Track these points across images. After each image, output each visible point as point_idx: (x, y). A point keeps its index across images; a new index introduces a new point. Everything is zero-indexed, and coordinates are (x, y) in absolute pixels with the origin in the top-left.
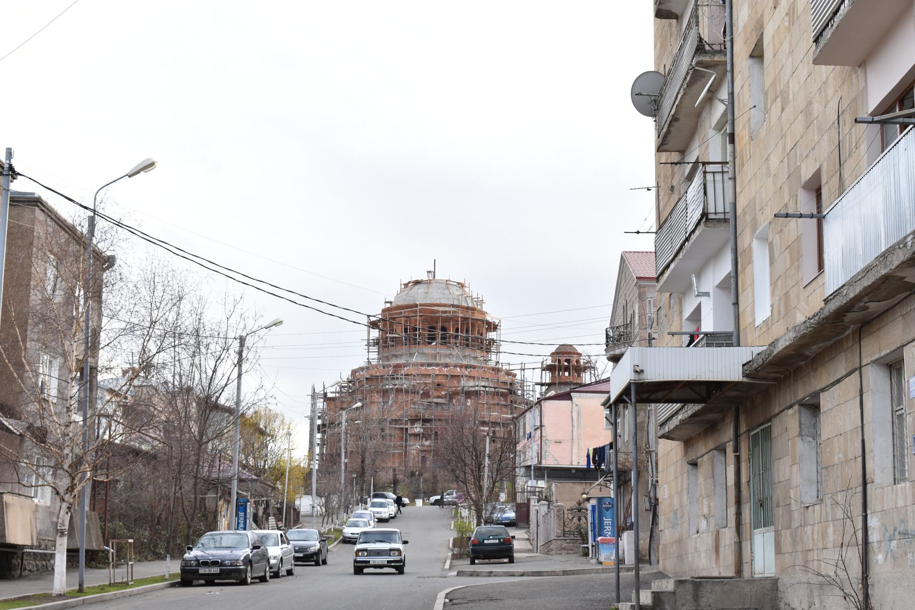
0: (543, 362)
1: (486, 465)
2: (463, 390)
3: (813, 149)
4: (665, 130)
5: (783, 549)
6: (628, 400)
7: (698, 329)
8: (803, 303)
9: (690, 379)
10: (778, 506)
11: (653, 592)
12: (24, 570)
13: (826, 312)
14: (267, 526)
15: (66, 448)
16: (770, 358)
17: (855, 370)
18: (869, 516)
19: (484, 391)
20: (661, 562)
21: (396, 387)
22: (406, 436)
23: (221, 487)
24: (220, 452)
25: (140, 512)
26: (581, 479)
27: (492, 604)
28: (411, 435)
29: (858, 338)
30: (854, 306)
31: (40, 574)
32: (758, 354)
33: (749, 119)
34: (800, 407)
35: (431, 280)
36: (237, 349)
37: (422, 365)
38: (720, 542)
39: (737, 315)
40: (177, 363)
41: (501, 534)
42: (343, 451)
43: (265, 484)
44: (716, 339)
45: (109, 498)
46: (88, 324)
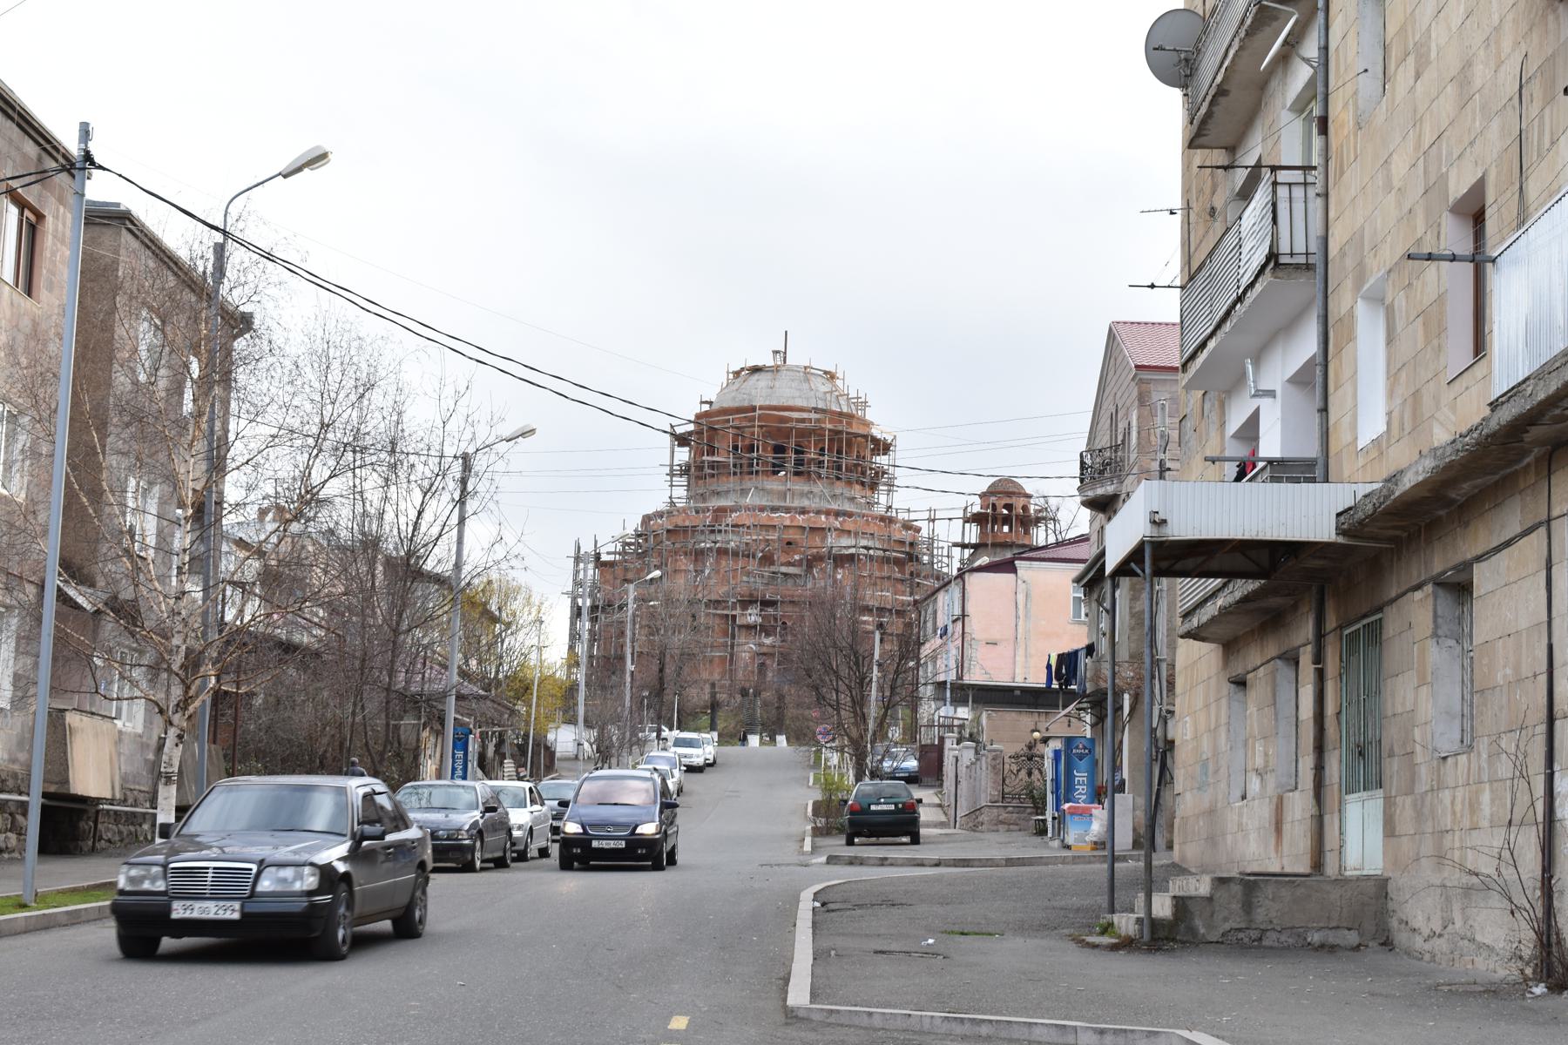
0: (966, 508)
1: (874, 679)
2: (830, 552)
3: (1471, 144)
4: (1203, 110)
5: (1398, 829)
6: (1139, 571)
7: (1254, 452)
8: (1445, 410)
9: (1246, 537)
10: (1391, 755)
11: (1174, 897)
12: (99, 840)
13: (1493, 425)
14: (500, 774)
15: (176, 635)
16: (1388, 503)
17: (1539, 525)
18: (1557, 776)
19: (866, 556)
20: (1176, 847)
21: (718, 545)
22: (733, 629)
23: (428, 709)
24: (426, 647)
25: (292, 746)
26: (1029, 706)
27: (894, 910)
28: (741, 627)
29: (1547, 467)
30: (1543, 415)
31: (126, 846)
32: (1365, 496)
33: (1356, 93)
34: (1436, 587)
35: (778, 366)
36: (458, 476)
37: (762, 509)
38: (1284, 814)
39: (1324, 430)
40: (357, 497)
41: (898, 796)
42: (628, 651)
43: (499, 704)
44: (1285, 470)
45: (240, 723)
46: (214, 424)
